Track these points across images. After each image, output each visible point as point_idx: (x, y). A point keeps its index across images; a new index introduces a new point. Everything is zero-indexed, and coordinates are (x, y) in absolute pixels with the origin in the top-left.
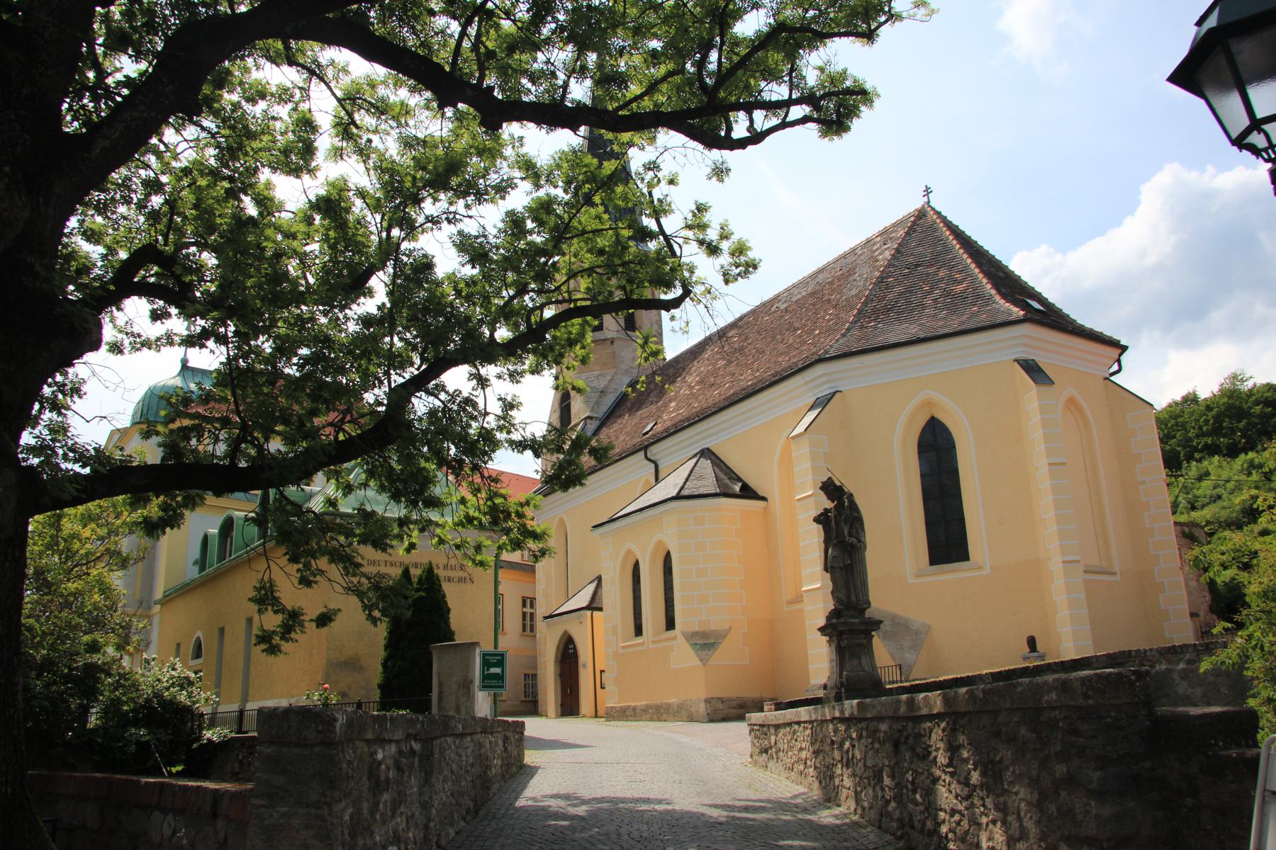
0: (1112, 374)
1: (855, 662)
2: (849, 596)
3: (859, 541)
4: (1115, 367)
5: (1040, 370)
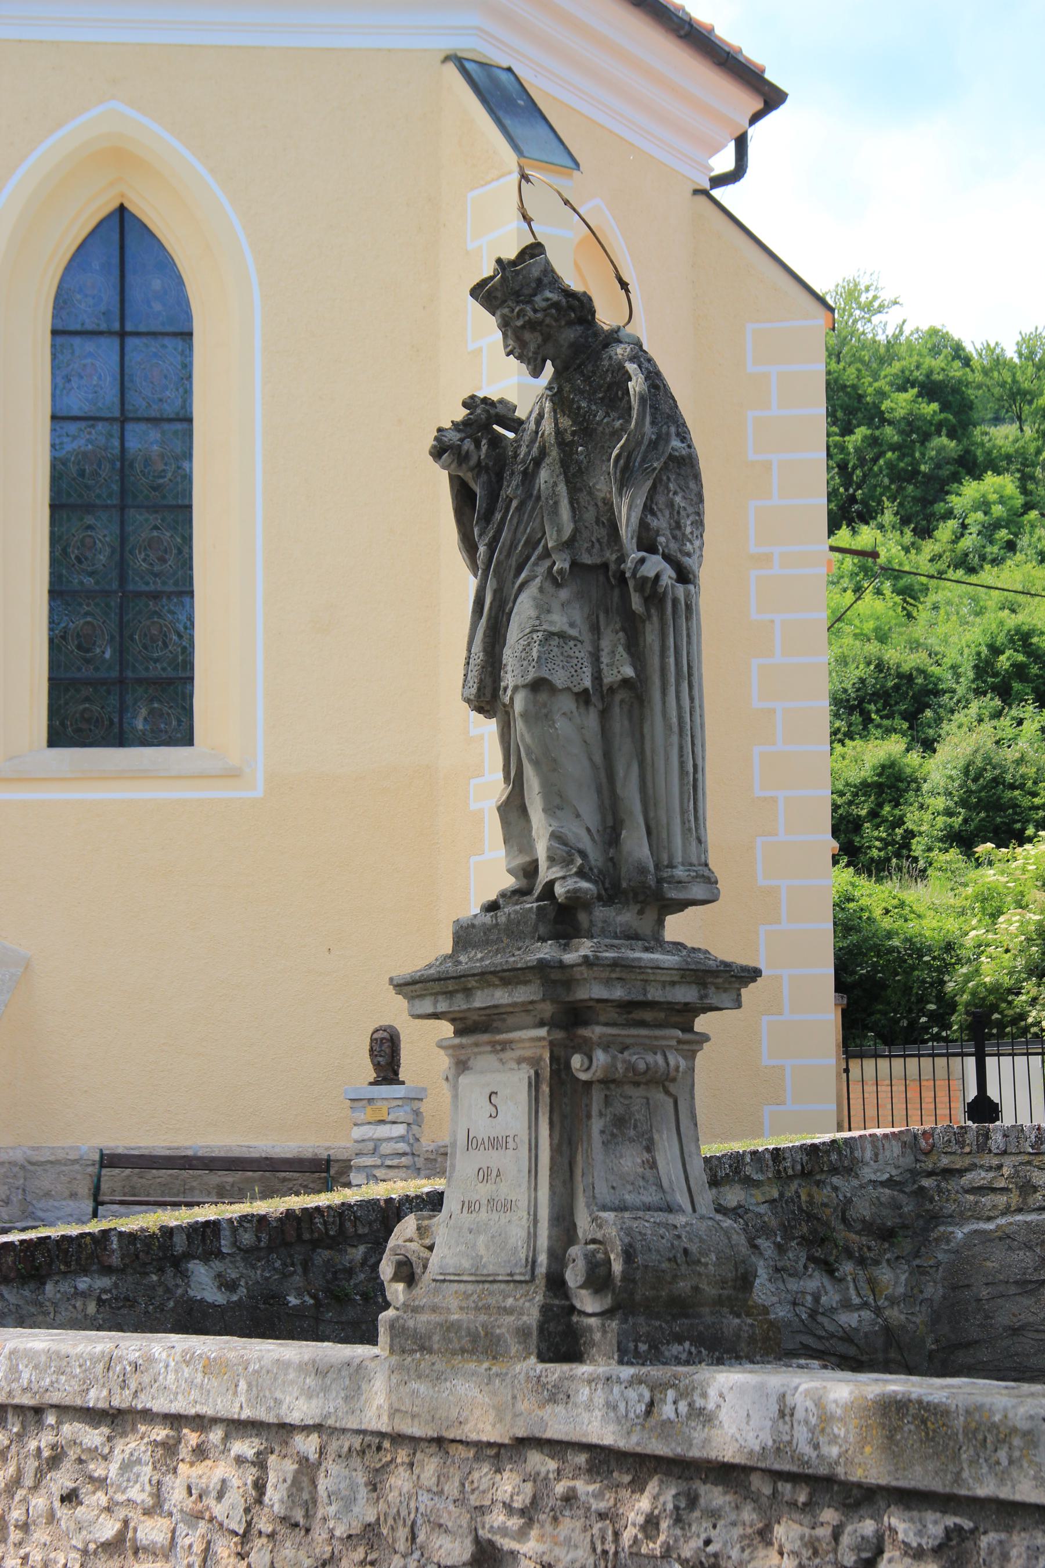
0: (720, 181)
1: (630, 1160)
2: (612, 833)
3: (684, 576)
4: (724, 161)
5: (534, 111)
